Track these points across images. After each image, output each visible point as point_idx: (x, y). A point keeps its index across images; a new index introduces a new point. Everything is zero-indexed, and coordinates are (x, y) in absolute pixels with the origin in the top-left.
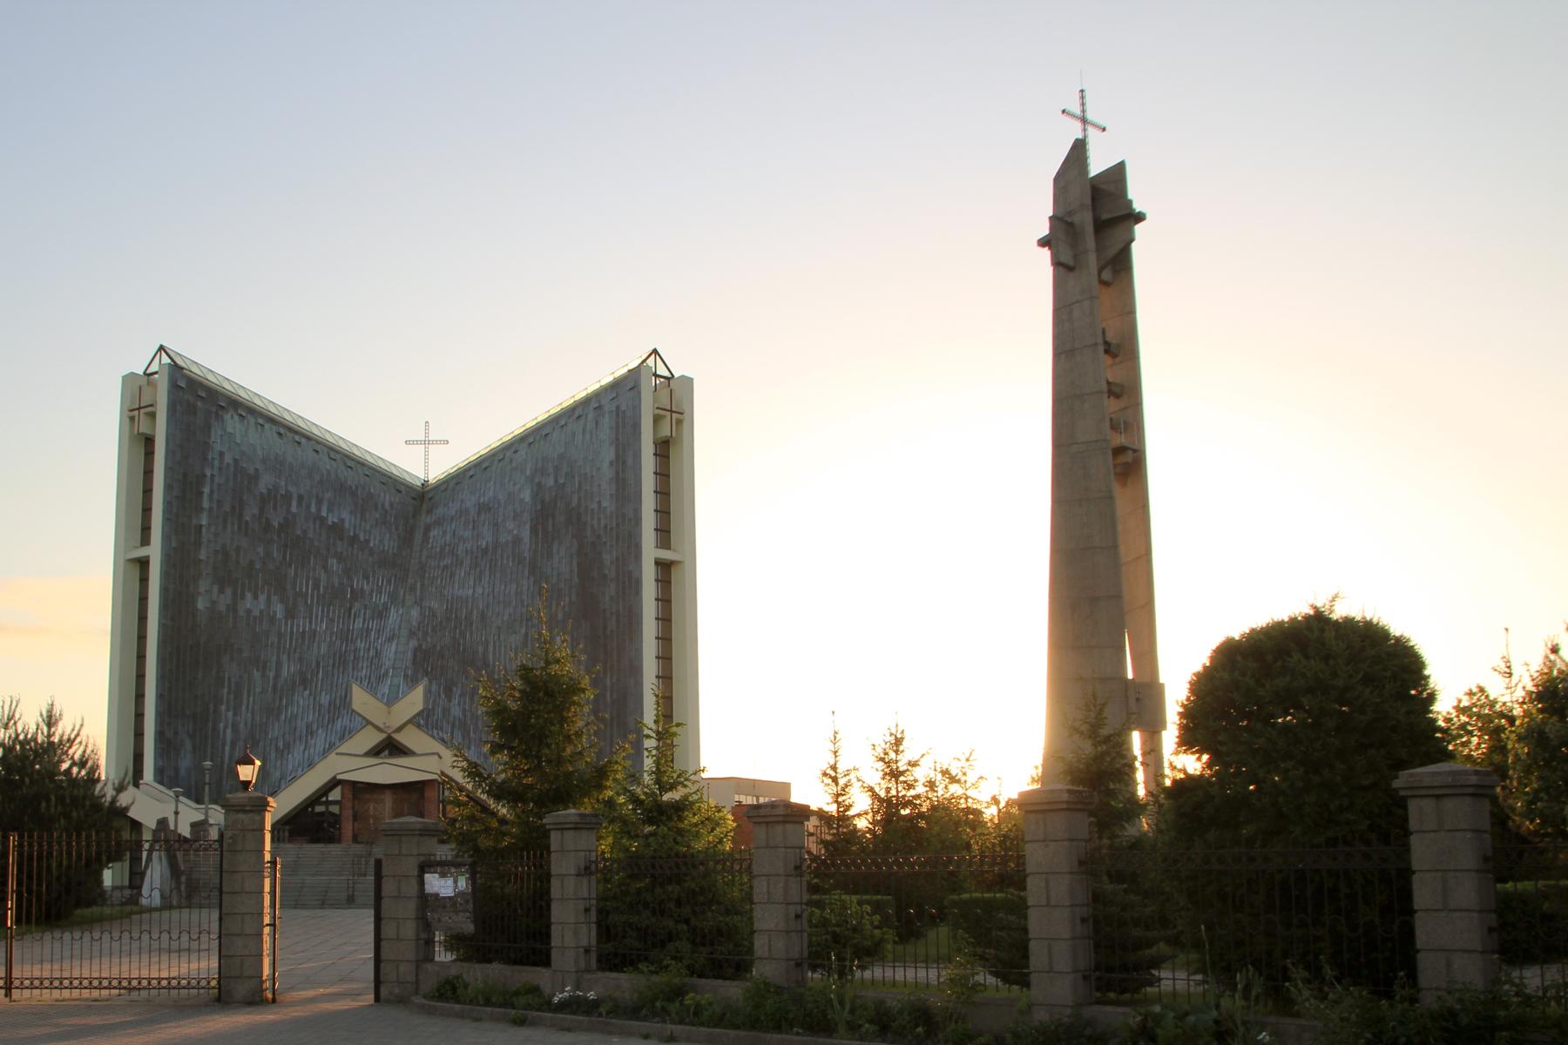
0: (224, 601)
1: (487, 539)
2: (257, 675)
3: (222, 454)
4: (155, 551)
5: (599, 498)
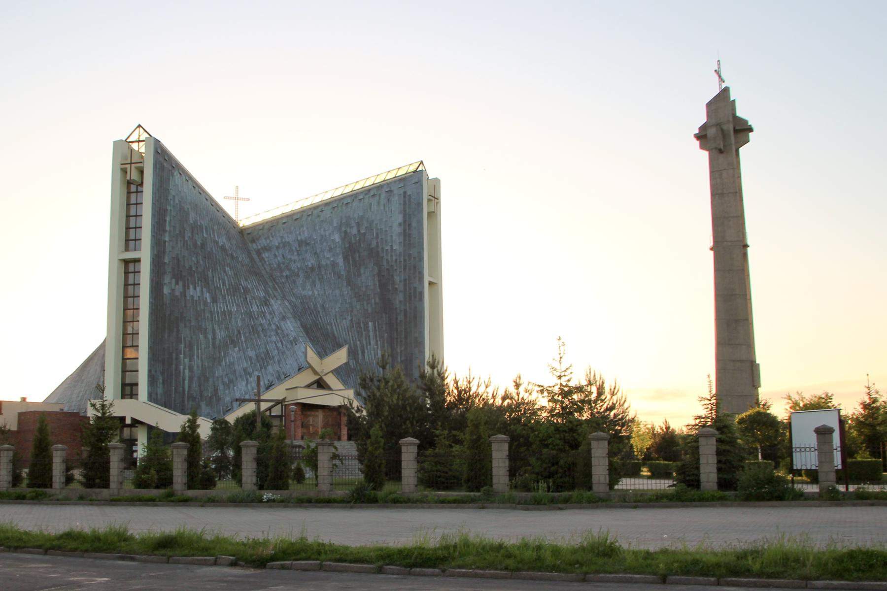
0: (179, 289)
1: (311, 262)
2: (201, 337)
3: (174, 197)
4: (145, 253)
5: (380, 245)
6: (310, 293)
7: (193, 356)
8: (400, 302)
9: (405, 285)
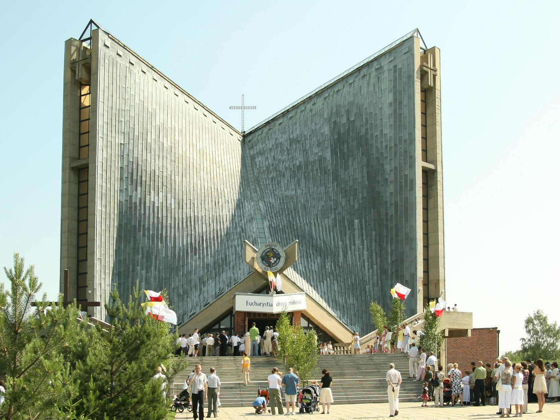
1: (299, 159)
6: (293, 193)
7: (151, 267)
8: (391, 193)
9: (395, 174)
